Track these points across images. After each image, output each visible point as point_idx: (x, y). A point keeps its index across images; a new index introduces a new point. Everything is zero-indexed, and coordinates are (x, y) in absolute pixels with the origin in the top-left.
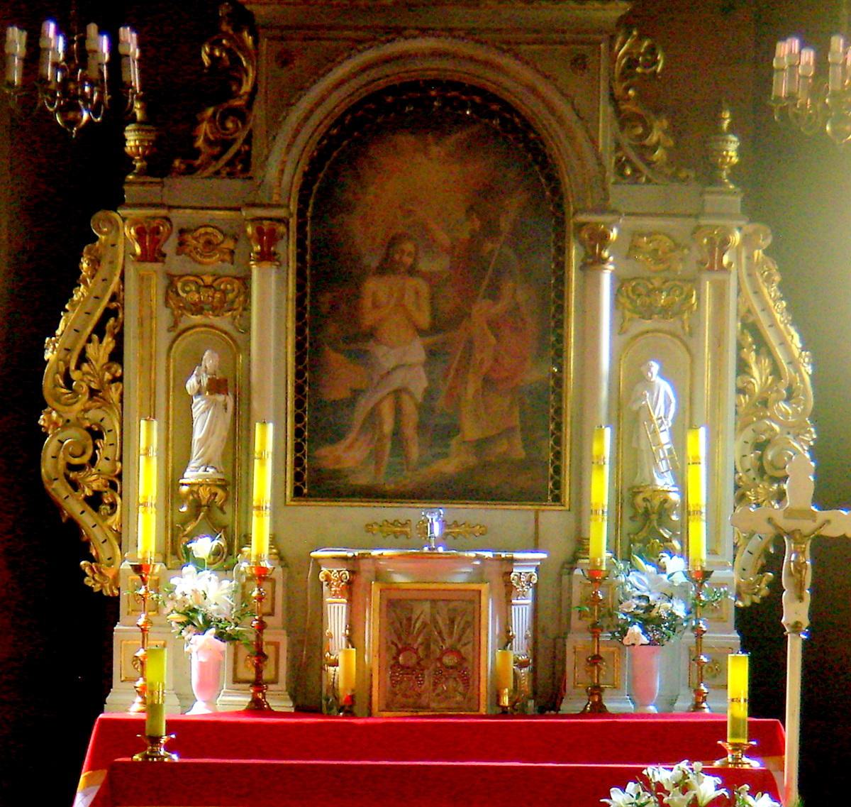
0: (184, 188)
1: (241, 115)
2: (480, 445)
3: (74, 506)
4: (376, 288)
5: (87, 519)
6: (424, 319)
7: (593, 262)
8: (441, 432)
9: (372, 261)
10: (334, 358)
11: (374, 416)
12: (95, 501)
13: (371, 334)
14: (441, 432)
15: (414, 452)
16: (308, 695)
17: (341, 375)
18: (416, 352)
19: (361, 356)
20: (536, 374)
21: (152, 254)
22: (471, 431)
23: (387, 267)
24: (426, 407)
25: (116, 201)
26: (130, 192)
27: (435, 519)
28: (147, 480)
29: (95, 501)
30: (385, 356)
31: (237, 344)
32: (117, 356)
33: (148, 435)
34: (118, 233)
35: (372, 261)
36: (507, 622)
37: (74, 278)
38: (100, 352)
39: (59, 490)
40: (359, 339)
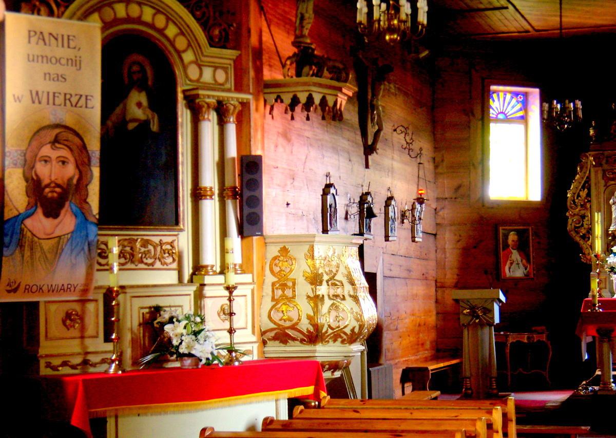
3: (578, 239)
21: (599, 164)
38: (583, 194)
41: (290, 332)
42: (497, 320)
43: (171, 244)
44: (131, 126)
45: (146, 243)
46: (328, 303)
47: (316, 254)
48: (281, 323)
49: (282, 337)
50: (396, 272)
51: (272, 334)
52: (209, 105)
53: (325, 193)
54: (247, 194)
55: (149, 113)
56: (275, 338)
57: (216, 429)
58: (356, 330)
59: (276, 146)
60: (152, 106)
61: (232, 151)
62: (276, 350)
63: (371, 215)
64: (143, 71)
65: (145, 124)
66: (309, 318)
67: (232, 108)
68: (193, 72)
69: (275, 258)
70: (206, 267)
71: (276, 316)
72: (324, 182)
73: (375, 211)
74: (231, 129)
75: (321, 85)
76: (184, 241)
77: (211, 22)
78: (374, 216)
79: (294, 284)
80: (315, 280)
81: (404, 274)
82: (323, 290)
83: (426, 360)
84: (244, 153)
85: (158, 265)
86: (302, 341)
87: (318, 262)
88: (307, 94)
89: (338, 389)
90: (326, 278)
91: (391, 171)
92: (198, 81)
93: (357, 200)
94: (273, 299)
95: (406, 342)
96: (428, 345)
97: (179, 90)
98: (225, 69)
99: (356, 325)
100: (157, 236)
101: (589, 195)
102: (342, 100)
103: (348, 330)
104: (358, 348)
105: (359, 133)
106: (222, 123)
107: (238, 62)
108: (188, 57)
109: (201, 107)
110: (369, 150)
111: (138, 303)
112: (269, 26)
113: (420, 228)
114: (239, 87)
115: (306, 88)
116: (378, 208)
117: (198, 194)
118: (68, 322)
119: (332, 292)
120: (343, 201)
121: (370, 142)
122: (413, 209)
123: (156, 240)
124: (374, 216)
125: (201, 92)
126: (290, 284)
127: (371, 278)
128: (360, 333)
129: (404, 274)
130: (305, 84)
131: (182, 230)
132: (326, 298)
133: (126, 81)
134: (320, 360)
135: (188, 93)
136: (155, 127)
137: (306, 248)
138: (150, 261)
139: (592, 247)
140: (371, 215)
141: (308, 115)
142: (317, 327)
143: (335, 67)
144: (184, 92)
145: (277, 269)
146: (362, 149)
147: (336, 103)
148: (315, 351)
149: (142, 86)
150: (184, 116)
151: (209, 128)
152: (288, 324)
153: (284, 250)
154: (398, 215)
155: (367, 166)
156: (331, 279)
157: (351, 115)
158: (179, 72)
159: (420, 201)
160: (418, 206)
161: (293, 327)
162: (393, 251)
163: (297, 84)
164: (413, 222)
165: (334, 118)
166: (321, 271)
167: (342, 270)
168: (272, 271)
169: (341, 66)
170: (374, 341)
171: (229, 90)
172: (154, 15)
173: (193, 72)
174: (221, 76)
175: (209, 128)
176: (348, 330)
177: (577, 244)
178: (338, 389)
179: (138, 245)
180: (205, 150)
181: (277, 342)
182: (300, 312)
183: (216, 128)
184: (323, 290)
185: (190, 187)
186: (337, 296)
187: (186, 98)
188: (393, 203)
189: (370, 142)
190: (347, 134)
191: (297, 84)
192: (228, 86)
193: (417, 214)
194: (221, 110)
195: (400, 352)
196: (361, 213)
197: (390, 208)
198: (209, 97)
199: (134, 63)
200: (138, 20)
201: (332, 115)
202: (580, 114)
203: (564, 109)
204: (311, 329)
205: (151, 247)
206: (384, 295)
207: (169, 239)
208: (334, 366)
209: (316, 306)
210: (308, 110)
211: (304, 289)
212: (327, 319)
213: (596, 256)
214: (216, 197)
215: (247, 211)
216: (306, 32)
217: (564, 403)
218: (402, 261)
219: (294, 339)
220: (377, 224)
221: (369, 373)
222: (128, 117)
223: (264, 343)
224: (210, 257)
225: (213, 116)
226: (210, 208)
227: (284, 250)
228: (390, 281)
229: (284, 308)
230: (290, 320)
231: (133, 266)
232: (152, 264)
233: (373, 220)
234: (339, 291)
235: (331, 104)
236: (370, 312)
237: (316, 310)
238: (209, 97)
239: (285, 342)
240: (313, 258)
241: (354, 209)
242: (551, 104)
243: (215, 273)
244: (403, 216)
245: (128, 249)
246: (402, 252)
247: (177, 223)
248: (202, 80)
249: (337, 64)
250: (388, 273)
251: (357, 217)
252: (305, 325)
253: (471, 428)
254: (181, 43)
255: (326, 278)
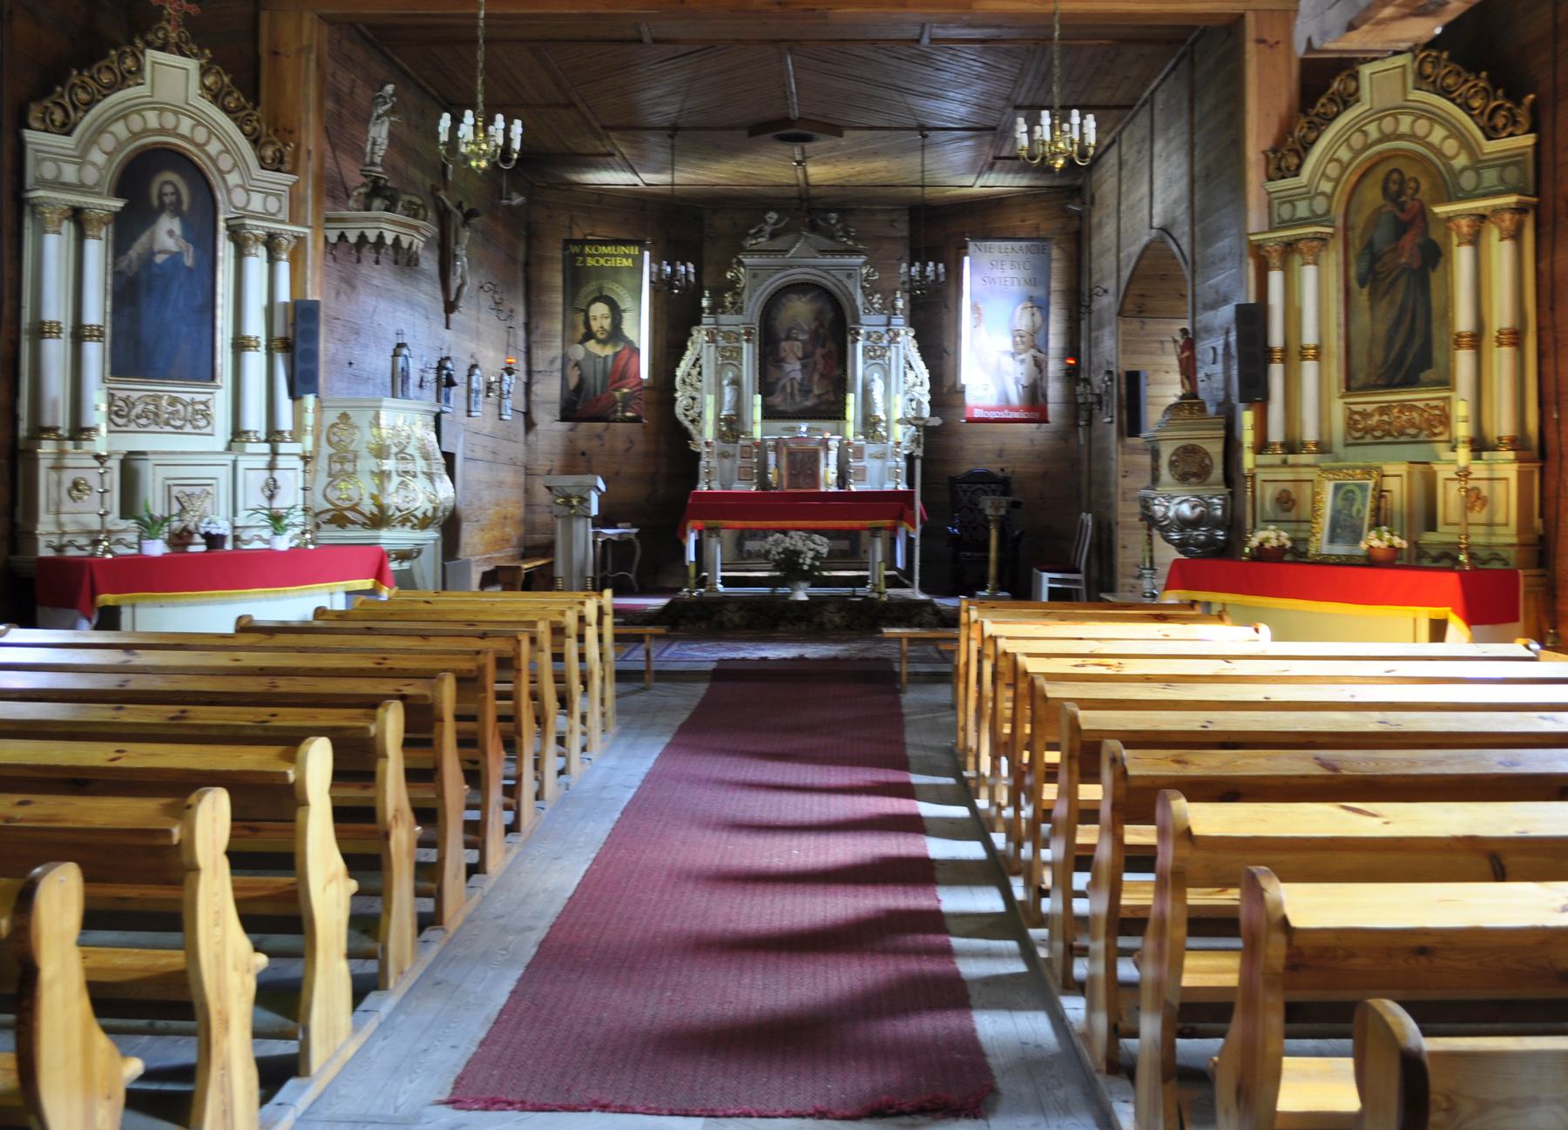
0: (723, 318)
1: (739, 294)
2: (819, 396)
3: (686, 423)
4: (785, 345)
5: (691, 427)
6: (800, 354)
7: (855, 341)
8: (806, 392)
9: (783, 336)
10: (771, 368)
11: (784, 387)
12: (693, 421)
13: (783, 360)
14: (806, 392)
15: (798, 399)
16: (763, 482)
17: (773, 373)
18: (798, 365)
19: (780, 368)
20: (838, 372)
21: (713, 340)
22: (816, 391)
23: (788, 338)
24: (801, 384)
25: (699, 323)
26: (705, 321)
27: (804, 426)
28: (709, 415)
29: (693, 421)
30: (788, 367)
31: (738, 368)
32: (700, 374)
33: (710, 400)
34: (699, 336)
35: (783, 336)
36: (13, 525)
37: (685, 348)
38: (695, 372)
39: (681, 417)
40: (779, 362)
41: (349, 514)
42: (594, 511)
43: (205, 403)
44: (160, 259)
45: (173, 401)
46: (396, 480)
47: (383, 422)
48: (339, 503)
49: (339, 519)
50: (479, 454)
51: (327, 516)
52: (257, 238)
53: (395, 355)
54: (300, 346)
55: (182, 243)
56: (330, 522)
57: (256, 618)
58: (429, 514)
59: (338, 293)
60: (187, 236)
61: (284, 295)
62: (331, 535)
63: (450, 383)
64: (177, 193)
65: (176, 257)
66: (373, 497)
67: (285, 242)
68: (239, 197)
69: (333, 426)
70: (247, 432)
71: (332, 495)
72: (395, 340)
73: (456, 380)
74: (284, 268)
75: (394, 222)
76: (220, 401)
77: (263, 140)
78: (454, 384)
79: (356, 457)
80: (381, 452)
81: (489, 457)
82: (389, 465)
83: (513, 558)
84: (299, 297)
85: (188, 428)
86: (363, 525)
87: (384, 432)
88: (377, 232)
89: (406, 581)
90: (394, 450)
91: (477, 335)
92: (244, 208)
93: (435, 365)
94: (330, 475)
95: (488, 536)
96: (514, 541)
97: (221, 217)
98: (278, 196)
99: (429, 506)
100: (189, 393)
101: (700, 374)
102: (419, 243)
103: (419, 514)
104: (431, 535)
105: (438, 286)
106: (272, 260)
107: (293, 189)
108: (233, 179)
109: (246, 239)
110: (450, 307)
111: (162, 472)
112: (334, 150)
113: (508, 403)
114: (293, 219)
115: (376, 224)
116: (459, 376)
117: (240, 345)
118: (75, 493)
119: (402, 467)
120: (419, 363)
121: (452, 298)
122: (501, 380)
123: (187, 397)
124: (454, 384)
125: (248, 221)
126: (351, 456)
127: (449, 458)
128: (434, 517)
129: (489, 457)
130: (377, 220)
131: (218, 387)
132: (394, 475)
133: (155, 202)
134: (386, 548)
135: (232, 223)
136: (189, 261)
137: (371, 413)
138: (178, 423)
139: (701, 432)
140: (450, 383)
141: (271, 497)
142: (381, 507)
143: (411, 203)
144: (227, 220)
145: (335, 439)
146: (442, 306)
147: (411, 244)
148: (378, 538)
149: (176, 211)
150: (225, 250)
151: (256, 265)
152: (347, 504)
153: (344, 417)
154: (482, 387)
155: (447, 327)
156: (401, 452)
157: (429, 263)
158: (220, 196)
159: (509, 371)
160: (506, 377)
161: (353, 509)
162: (478, 426)
163: (366, 219)
164: (501, 396)
165: (408, 264)
166: (388, 442)
167: (414, 442)
168: (329, 441)
169: (419, 202)
170: (450, 525)
171: (282, 222)
172: (193, 127)
173: (239, 197)
174: (273, 205)
175: (256, 265)
176: (419, 514)
177: (686, 429)
178: (406, 581)
179: (164, 403)
180: (250, 291)
181: (333, 526)
182: (361, 490)
183: (265, 266)
184: (389, 465)
185: (230, 335)
186: (406, 472)
187: (228, 227)
188: (477, 372)
189: (452, 298)
190: (425, 286)
191: (366, 219)
192: (280, 217)
193: (505, 387)
194: (271, 243)
195: (478, 548)
196: (438, 379)
197: (474, 378)
198: (258, 227)
199: (167, 183)
200: (146, 131)
201: (405, 260)
202: (692, 278)
203: (674, 271)
204: (375, 510)
205: (180, 407)
206: (464, 480)
207: (203, 398)
208: (403, 556)
209: (382, 483)
210: (378, 252)
211: (367, 464)
212: (394, 499)
213: (707, 444)
214: (262, 349)
215: (300, 366)
216: (378, 160)
217: (666, 608)
218: (489, 443)
219: (353, 523)
220: (457, 393)
221: (444, 567)
222: (156, 248)
223: (318, 526)
224: (254, 420)
225: (262, 251)
226: (255, 362)
227: (344, 417)
228: (471, 464)
229: (342, 485)
230: (349, 499)
231: (157, 429)
232: (180, 427)
233: (454, 389)
234: (410, 467)
235: (405, 245)
236: (445, 490)
237: (381, 488)
238: (257, 227)
239: (342, 526)
240: (378, 425)
241: (431, 376)
242: (660, 265)
243: (259, 441)
244: (489, 388)
245: (151, 407)
246: (486, 431)
247: (213, 378)
248: (250, 208)
249: (415, 199)
250: (469, 455)
251: (434, 385)
252: (368, 507)
253: (559, 618)
254: (225, 162)
255: (394, 450)
